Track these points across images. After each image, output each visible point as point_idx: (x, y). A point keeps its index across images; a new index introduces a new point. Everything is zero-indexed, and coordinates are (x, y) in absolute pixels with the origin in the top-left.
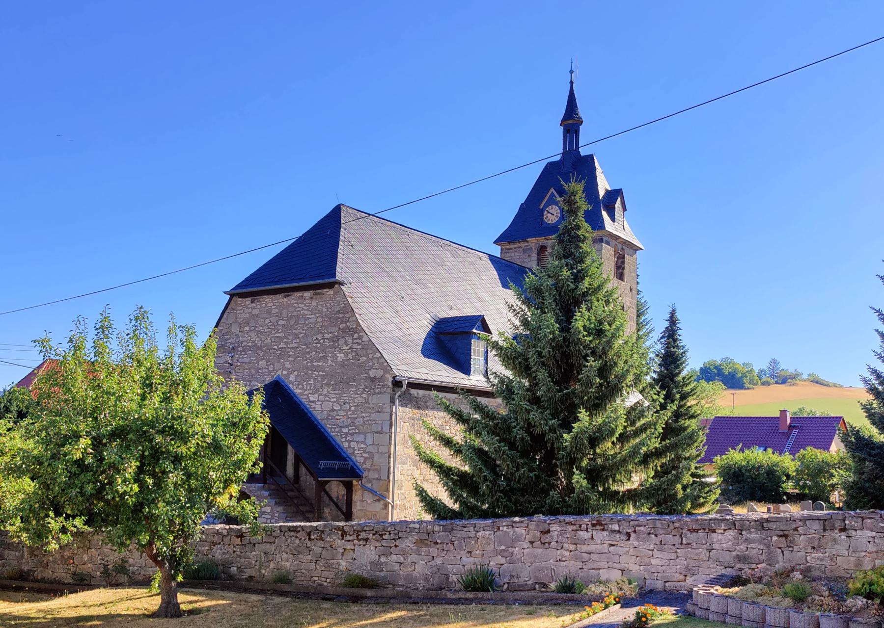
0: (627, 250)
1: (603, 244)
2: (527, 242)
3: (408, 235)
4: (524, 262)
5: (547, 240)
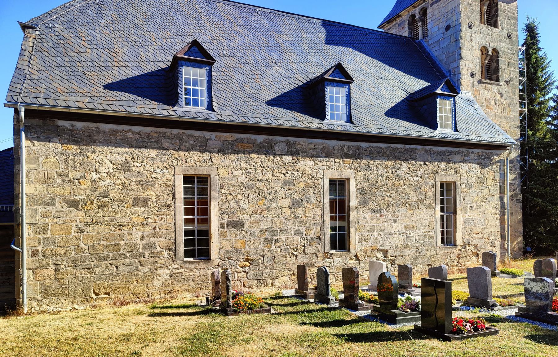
2: (401, 16)
5: (415, 7)
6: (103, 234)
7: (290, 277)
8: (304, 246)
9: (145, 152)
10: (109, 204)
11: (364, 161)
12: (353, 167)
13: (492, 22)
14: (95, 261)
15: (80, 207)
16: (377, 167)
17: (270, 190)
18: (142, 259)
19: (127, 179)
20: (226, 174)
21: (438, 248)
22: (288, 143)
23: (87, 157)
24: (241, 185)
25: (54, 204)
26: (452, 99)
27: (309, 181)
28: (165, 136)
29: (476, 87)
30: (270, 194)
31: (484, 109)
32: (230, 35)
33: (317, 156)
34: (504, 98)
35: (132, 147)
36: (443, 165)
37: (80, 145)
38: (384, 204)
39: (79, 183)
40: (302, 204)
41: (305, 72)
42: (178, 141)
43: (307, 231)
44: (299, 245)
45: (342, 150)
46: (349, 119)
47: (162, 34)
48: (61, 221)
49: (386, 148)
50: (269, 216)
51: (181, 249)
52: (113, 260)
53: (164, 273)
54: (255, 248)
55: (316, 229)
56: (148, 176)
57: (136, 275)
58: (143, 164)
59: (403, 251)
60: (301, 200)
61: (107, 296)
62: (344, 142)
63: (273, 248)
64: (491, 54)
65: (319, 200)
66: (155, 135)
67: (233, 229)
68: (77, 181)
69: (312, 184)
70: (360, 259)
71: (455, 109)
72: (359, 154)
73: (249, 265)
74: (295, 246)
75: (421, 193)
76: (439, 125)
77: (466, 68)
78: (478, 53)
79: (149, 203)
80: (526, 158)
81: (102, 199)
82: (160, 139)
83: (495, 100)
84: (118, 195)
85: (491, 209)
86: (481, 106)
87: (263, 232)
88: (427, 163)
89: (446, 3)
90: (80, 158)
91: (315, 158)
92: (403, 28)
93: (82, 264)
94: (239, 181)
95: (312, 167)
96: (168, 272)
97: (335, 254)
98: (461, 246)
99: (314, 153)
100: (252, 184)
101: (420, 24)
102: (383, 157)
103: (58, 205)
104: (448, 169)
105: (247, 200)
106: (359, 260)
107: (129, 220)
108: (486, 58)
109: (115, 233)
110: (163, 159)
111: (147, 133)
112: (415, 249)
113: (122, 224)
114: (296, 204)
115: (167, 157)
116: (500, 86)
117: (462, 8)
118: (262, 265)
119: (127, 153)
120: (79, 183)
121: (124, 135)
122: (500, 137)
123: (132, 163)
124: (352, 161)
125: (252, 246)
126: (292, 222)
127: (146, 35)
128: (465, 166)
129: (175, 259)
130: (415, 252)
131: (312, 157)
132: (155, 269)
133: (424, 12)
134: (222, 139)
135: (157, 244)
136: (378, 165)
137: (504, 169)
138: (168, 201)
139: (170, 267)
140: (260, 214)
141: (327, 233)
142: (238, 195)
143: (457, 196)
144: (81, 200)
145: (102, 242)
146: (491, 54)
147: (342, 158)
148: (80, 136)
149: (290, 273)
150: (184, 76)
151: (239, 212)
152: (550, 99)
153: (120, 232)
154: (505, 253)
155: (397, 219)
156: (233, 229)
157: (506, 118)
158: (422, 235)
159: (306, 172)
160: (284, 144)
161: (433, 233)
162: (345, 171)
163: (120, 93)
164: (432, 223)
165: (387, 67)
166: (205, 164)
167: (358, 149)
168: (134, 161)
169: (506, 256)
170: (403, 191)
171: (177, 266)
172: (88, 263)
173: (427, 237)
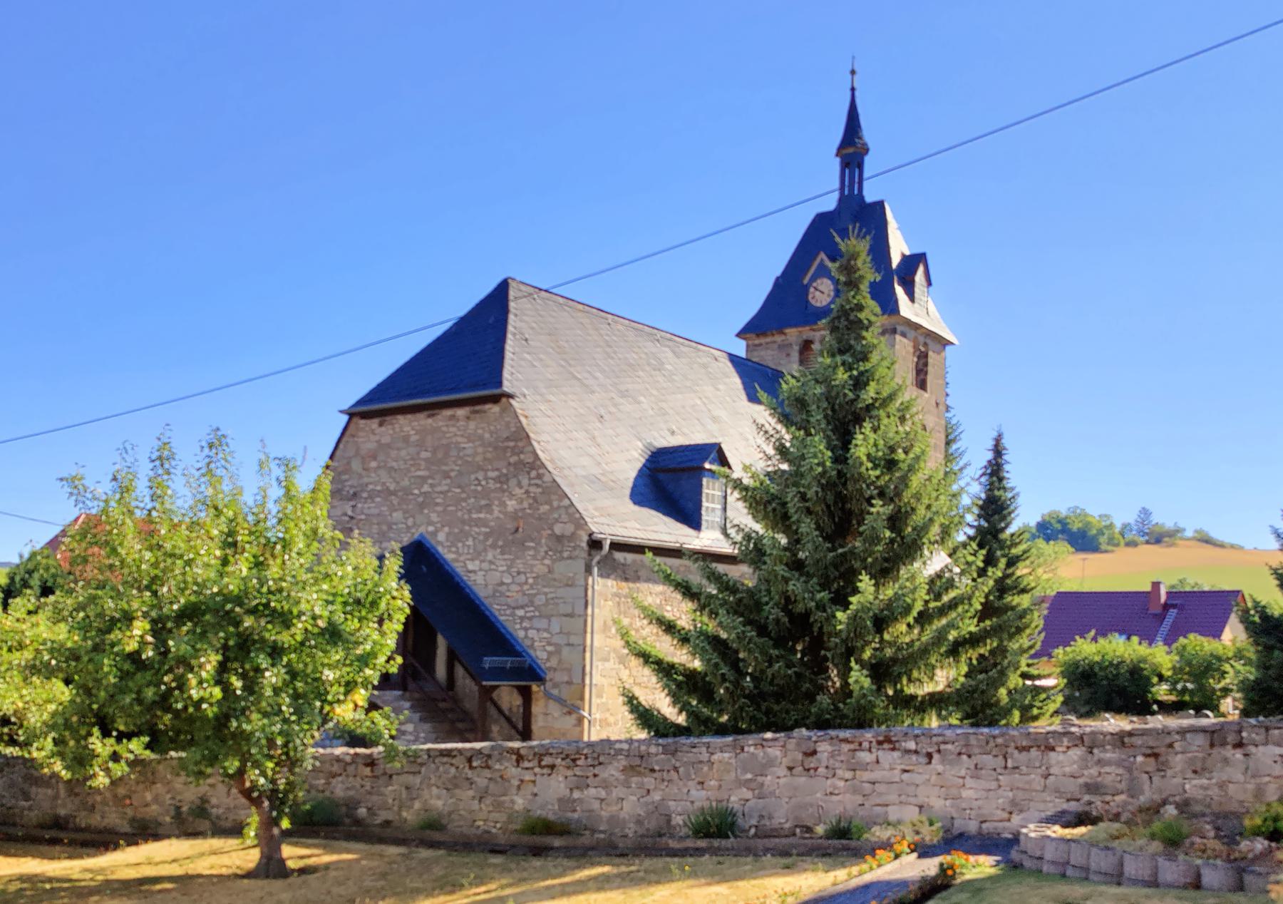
2: (785, 334)
4: (780, 364)
103: (612, 661)
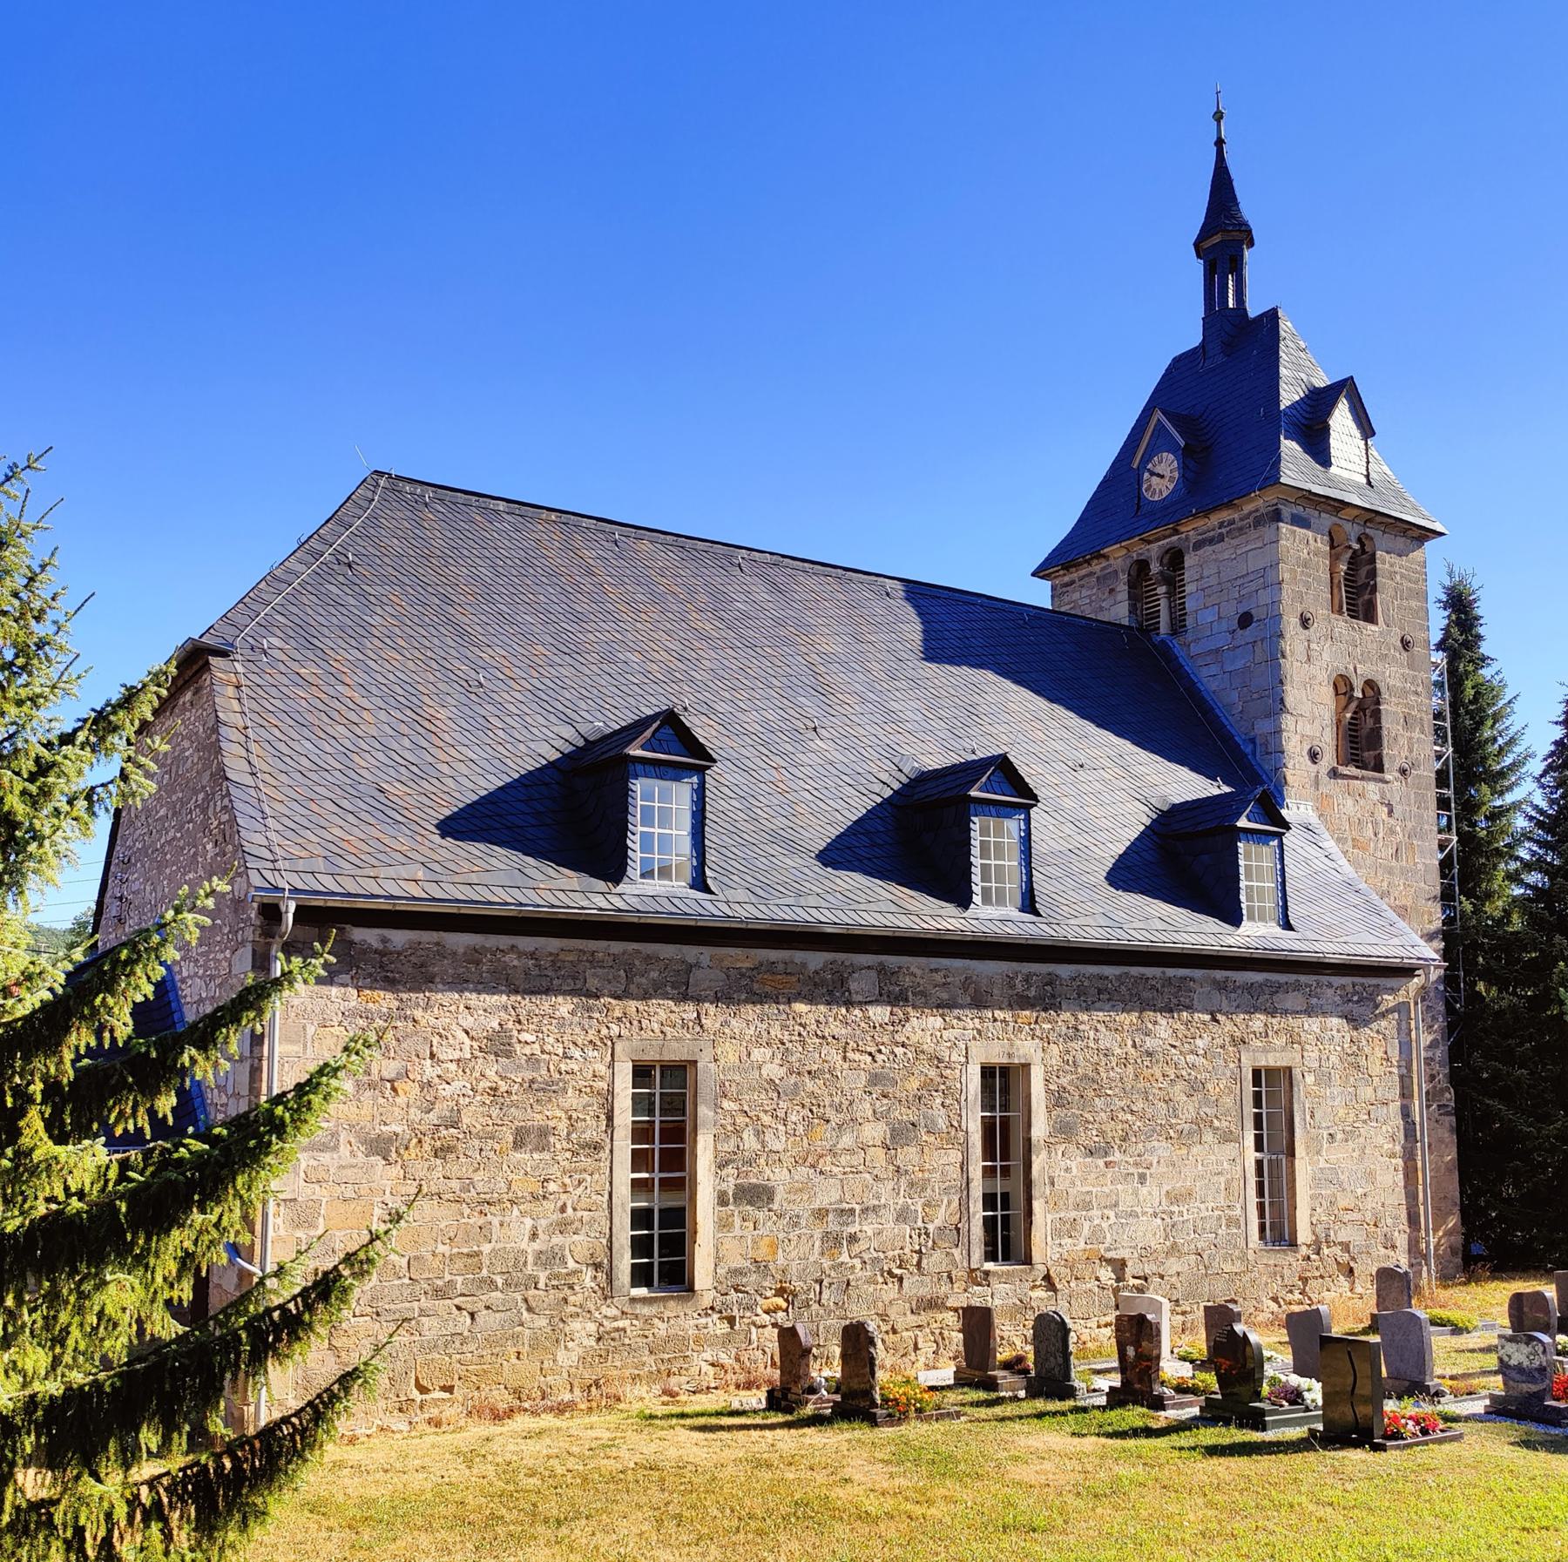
0: (1380, 538)
1: (1281, 524)
2: (1106, 557)
3: (616, 542)
4: (1101, 609)
5: (1149, 542)
6: (442, 1226)
7: (886, 1337)
8: (920, 1252)
9: (545, 1003)
10: (460, 1145)
11: (1066, 1016)
12: (1038, 1033)
13: (1360, 601)
14: (423, 1299)
15: (394, 1155)
16: (1097, 1030)
17: (837, 1100)
18: (532, 1292)
19: (503, 1078)
20: (732, 1058)
21: (1250, 1252)
22: (882, 970)
23: (414, 1021)
24: (767, 1086)
25: (336, 1148)
26: (1275, 843)
27: (932, 1073)
28: (593, 962)
29: (1323, 789)
30: (839, 1109)
31: (1346, 848)
32: (686, 643)
33: (951, 1005)
34: (1396, 816)
35: (517, 992)
36: (1258, 1022)
37: (398, 991)
38: (1114, 1130)
39: (394, 1089)
40: (916, 1136)
41: (891, 753)
42: (622, 973)
43: (927, 1210)
44: (907, 1250)
45: (1013, 987)
46: (1027, 902)
47: (526, 653)
48: (349, 1194)
49: (1119, 977)
50: (836, 1170)
51: (625, 1262)
52: (464, 1295)
53: (582, 1329)
54: (800, 1259)
55: (949, 1203)
56: (552, 1067)
57: (516, 1337)
58: (540, 1035)
59: (1163, 1263)
60: (913, 1124)
61: (446, 1395)
62: (1015, 965)
63: (845, 1258)
64: (1360, 696)
65: (956, 1124)
66: (571, 959)
67: (748, 1207)
68: (388, 1085)
69: (939, 1079)
70: (1058, 1287)
71: (1283, 870)
72: (1053, 996)
73: (784, 1305)
74: (896, 1252)
75: (1206, 1101)
76: (1244, 912)
77: (1298, 737)
78: (1327, 693)
79: (552, 1139)
80: (1458, 976)
81: (444, 1132)
82: (580, 968)
83: (1375, 824)
84: (481, 1120)
85: (1380, 1140)
86: (1339, 840)
87: (821, 1214)
88: (1219, 1017)
89: (1239, 552)
90: (399, 1024)
91: (946, 1010)
92: (1112, 591)
93: (393, 1307)
94: (765, 1076)
95: (939, 1034)
96: (592, 1327)
97: (995, 1273)
98: (1309, 1246)
99: (945, 996)
100: (796, 1084)
101: (1162, 589)
102: (1111, 1003)
103: (344, 1150)
104: (1270, 1033)
105: (781, 1128)
106: (1055, 1290)
107: (503, 1186)
108: (1346, 707)
109: (471, 1221)
110: (586, 1022)
111: (551, 954)
112: (1194, 1257)
113: (488, 1196)
114: (900, 1135)
115: (597, 1015)
116: (1387, 782)
117: (1285, 573)
118: (815, 1306)
119: (505, 1008)
120: (394, 1089)
121: (499, 960)
122: (1396, 941)
123: (515, 1033)
124: (1035, 1014)
125: (794, 1254)
126: (891, 1185)
127: (488, 659)
128: (1313, 1024)
129: (607, 1292)
130: (1193, 1264)
131: (938, 1007)
132: (562, 1320)
133: (1175, 559)
134: (726, 963)
135: (567, 1252)
136: (1099, 1026)
137: (1410, 1031)
138: (595, 1133)
139: (597, 1315)
140: (813, 1166)
141: (974, 1214)
142: (762, 1115)
143: (1296, 1106)
144: (397, 1135)
145: (441, 1249)
146: (1360, 696)
147: (1010, 1006)
148: (399, 965)
149: (884, 1328)
150: (639, 803)
151: (762, 1161)
152: (1516, 806)
153: (481, 1221)
154: (1420, 1264)
155: (1148, 1172)
156: (749, 1208)
157: (1404, 871)
158: (1211, 1217)
159: (925, 1047)
160: (873, 974)
161: (1238, 1212)
162: (1019, 1042)
163: (481, 846)
164: (1235, 1184)
165: (1090, 728)
166: (685, 1031)
167: (1050, 983)
168: (519, 1027)
169: (1425, 1275)
170: (1162, 1094)
171: (612, 1312)
172: (408, 1305)
173: (1224, 1222)
